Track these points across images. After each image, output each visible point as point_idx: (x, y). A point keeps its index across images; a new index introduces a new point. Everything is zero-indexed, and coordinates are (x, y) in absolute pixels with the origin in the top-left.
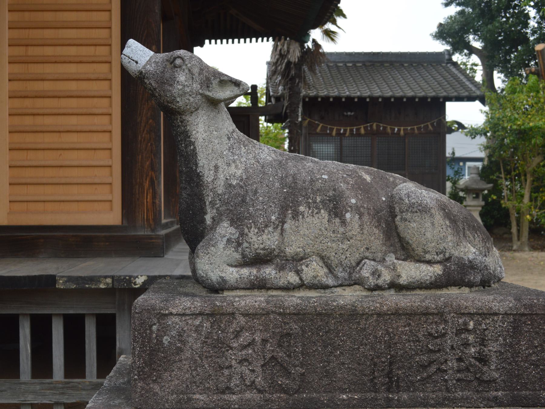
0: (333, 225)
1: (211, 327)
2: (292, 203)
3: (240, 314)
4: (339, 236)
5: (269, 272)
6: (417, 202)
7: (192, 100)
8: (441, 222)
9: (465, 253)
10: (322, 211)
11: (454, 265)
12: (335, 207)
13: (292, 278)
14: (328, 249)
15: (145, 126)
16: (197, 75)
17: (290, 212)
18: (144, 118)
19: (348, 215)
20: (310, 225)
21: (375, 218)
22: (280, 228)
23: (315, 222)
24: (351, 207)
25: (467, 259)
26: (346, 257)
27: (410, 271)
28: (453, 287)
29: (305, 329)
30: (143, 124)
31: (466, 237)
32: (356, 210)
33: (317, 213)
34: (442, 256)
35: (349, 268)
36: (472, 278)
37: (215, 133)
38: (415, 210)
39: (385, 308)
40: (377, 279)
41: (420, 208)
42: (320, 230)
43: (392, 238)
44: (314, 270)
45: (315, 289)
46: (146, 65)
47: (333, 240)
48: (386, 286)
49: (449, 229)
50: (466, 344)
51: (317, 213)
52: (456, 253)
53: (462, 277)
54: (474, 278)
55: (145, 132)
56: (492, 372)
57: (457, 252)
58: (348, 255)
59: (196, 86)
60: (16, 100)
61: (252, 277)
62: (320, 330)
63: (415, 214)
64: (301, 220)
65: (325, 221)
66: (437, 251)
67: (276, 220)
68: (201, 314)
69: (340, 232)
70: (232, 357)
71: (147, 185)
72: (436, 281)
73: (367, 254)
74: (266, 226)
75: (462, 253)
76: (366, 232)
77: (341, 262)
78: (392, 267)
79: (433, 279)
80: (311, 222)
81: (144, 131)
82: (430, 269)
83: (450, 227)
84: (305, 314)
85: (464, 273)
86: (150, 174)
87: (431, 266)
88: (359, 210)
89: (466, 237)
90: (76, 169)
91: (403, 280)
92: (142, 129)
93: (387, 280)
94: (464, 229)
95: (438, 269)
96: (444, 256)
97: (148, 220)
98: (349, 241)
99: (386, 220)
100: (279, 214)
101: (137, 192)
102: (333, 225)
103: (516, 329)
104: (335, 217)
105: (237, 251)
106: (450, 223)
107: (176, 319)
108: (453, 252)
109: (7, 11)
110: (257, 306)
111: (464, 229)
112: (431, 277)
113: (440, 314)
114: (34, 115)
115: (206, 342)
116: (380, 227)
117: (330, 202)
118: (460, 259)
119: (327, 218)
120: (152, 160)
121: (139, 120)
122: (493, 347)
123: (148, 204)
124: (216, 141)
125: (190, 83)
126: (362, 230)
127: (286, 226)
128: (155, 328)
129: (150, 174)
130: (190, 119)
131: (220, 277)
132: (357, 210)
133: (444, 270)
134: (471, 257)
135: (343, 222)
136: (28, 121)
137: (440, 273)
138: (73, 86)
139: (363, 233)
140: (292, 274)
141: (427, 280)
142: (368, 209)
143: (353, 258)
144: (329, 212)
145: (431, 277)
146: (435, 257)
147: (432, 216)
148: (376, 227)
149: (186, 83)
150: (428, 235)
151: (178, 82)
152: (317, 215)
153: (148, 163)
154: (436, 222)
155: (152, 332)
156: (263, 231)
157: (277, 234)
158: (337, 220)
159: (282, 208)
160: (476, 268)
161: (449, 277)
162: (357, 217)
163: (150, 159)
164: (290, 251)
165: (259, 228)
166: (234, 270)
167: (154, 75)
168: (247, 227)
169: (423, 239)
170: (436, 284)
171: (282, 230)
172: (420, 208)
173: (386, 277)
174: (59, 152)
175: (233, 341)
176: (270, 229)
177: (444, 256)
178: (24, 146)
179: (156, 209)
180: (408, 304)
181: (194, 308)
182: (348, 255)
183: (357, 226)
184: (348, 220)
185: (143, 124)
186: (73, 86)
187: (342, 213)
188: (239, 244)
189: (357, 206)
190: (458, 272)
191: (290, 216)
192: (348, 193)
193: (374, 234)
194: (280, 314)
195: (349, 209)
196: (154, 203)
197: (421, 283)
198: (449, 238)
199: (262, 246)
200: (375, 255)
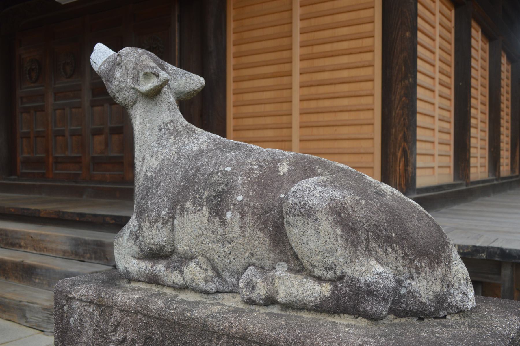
0: (213, 225)
1: (100, 316)
2: (183, 198)
3: (117, 309)
4: (218, 237)
5: (160, 268)
6: (300, 203)
7: (127, 94)
8: (329, 229)
9: (361, 274)
10: (204, 208)
11: (346, 287)
12: (218, 205)
13: (176, 278)
14: (210, 251)
15: (399, 103)
16: (131, 70)
17: (179, 207)
18: (398, 97)
19: (229, 215)
20: (191, 222)
21: (260, 219)
22: (170, 223)
23: (196, 220)
24: (234, 205)
25: (363, 281)
26: (230, 261)
27: (292, 286)
28: (346, 315)
29: (165, 335)
30: (397, 102)
31: (370, 252)
32: (239, 208)
33: (199, 210)
34: (332, 273)
35: (237, 274)
36: (369, 308)
37: (148, 125)
38: (297, 212)
39: (233, 330)
40: (251, 292)
41: (303, 210)
42: (200, 229)
43: (281, 244)
44: (194, 272)
45: (195, 292)
46: (101, 66)
47: (213, 242)
48: (261, 302)
49: (339, 240)
51: (199, 210)
52: (349, 272)
53: (354, 305)
54: (372, 308)
55: (399, 108)
57: (350, 270)
58: (232, 260)
59: (129, 81)
61: (148, 272)
62: (177, 340)
63: (297, 218)
64: (185, 216)
65: (205, 219)
66: (325, 266)
67: (166, 215)
68: (91, 302)
69: (219, 233)
71: (399, 154)
72: (321, 304)
73: (253, 260)
74: (156, 221)
75: (358, 273)
76: (247, 235)
77: (226, 266)
78: (271, 280)
79: (318, 301)
80: (193, 220)
81: (397, 108)
82: (317, 287)
83: (341, 237)
84: (165, 320)
85: (358, 299)
86: (403, 145)
87: (320, 284)
88: (242, 209)
89: (370, 252)
91: (281, 297)
92: (396, 106)
93: (261, 294)
94: (368, 240)
95: (326, 289)
96: (335, 273)
98: (230, 243)
99: (275, 222)
100: (170, 209)
101: (391, 160)
102: (213, 225)
104: (215, 216)
105: (135, 244)
106: (343, 231)
107: (78, 303)
108: (345, 269)
109: (299, 21)
110: (128, 304)
111: (368, 240)
112: (316, 298)
115: (97, 330)
116: (266, 230)
117: (215, 198)
118: (354, 280)
119: (207, 216)
120: (404, 132)
121: (393, 98)
123: (401, 171)
124: (148, 133)
125: (125, 78)
126: (243, 232)
127: (176, 222)
128: (65, 308)
129: (403, 145)
130: (132, 112)
131: (125, 268)
133: (333, 292)
134: (370, 278)
135: (223, 222)
136: (313, 104)
137: (328, 295)
138: (345, 74)
139: (244, 236)
140: (177, 274)
141: (311, 301)
142: (255, 208)
143: (238, 263)
144: (211, 210)
145: (316, 298)
146: (325, 273)
147: (316, 221)
148: (260, 230)
149: (121, 79)
150: (312, 245)
151: (115, 79)
152: (199, 212)
153: (400, 135)
154: (321, 230)
155: (63, 313)
156: (153, 226)
157: (165, 232)
158: (217, 219)
159: (174, 202)
160: (375, 295)
161: (337, 302)
162: (239, 216)
163: (403, 133)
165: (150, 223)
166: (135, 261)
167: (104, 74)
168: (143, 220)
169: (306, 249)
171: (173, 225)
172: (303, 210)
174: (335, 128)
175: (112, 334)
176: (159, 224)
177: (335, 273)
179: (408, 175)
180: (257, 331)
181: (88, 296)
182: (232, 260)
183: (237, 227)
184: (228, 220)
185: (397, 102)
186: (345, 74)
187: (223, 212)
188: (137, 238)
189: (242, 205)
190: (350, 297)
191: (178, 211)
192: (240, 187)
193: (258, 238)
194: (145, 315)
195: (232, 207)
196: (406, 170)
197: (305, 304)
198: (339, 252)
199: (152, 241)
200: (263, 262)
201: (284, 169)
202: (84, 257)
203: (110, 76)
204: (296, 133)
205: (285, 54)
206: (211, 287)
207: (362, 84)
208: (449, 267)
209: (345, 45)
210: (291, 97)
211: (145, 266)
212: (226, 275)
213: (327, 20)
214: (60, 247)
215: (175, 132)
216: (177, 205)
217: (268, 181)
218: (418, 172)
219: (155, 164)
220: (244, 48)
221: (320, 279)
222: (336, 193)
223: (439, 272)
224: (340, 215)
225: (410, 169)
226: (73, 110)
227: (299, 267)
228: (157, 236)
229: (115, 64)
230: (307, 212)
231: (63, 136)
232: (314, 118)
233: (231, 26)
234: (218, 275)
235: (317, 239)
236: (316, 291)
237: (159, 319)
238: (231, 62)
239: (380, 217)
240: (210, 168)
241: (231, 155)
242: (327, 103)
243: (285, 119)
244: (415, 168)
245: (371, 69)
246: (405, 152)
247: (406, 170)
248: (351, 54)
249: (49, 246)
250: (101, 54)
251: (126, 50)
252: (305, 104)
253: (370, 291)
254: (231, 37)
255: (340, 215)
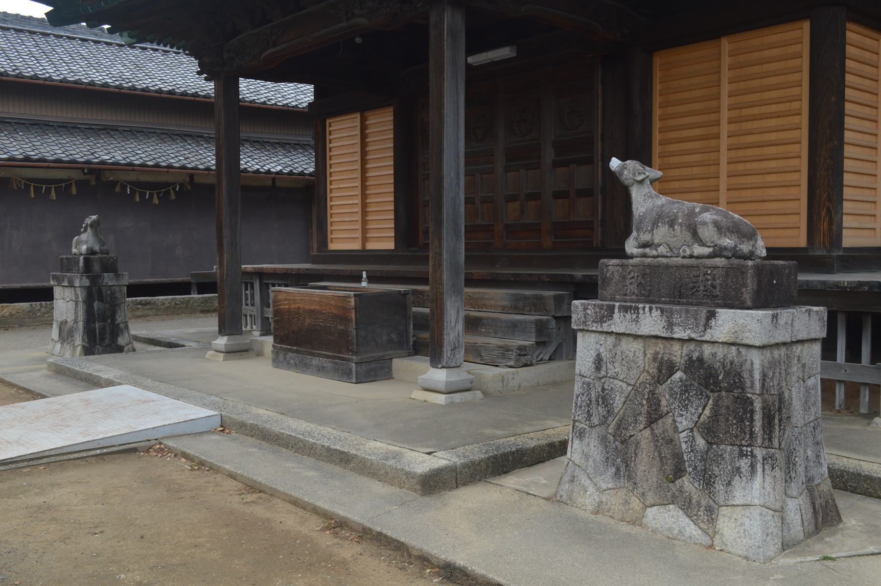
5: (647, 250)
13: (654, 253)
44: (662, 250)
50: (707, 280)
56: (717, 292)
60: (732, 151)
70: (628, 282)
71: (823, 213)
90: (775, 203)
91: (695, 254)
95: (711, 250)
97: (824, 243)
103: (727, 275)
113: (698, 267)
114: (745, 162)
122: (718, 281)
132: (681, 225)
135: (674, 230)
136: (741, 167)
138: (773, 136)
157: (650, 236)
164: (656, 241)
170: (710, 256)
173: (688, 253)
174: (763, 190)
178: (737, 187)
186: (773, 136)
196: (830, 229)
201: (697, 210)
202: (523, 310)
203: (621, 174)
204: (723, 196)
205: (713, 117)
206: (669, 254)
207: (790, 146)
208: (756, 242)
209: (773, 108)
210: (719, 160)
211: (640, 250)
212: (674, 250)
213: (756, 83)
214: (499, 303)
215: (651, 197)
216: (655, 224)
217: (692, 214)
218: (845, 232)
219: (644, 210)
220: (670, 110)
221: (709, 247)
222: (715, 217)
223: (751, 243)
224: (716, 224)
225: (834, 228)
226: (484, 176)
227: (703, 244)
228: (645, 237)
229: (623, 168)
230: (704, 223)
231: (474, 203)
232: (742, 180)
233: (657, 87)
234: (671, 250)
235: (707, 233)
236: (706, 251)
237: (649, 266)
238: (657, 124)
239: (730, 224)
240: (668, 211)
241: (676, 205)
242: (755, 166)
243: (712, 182)
244: (841, 228)
245: (798, 131)
246: (829, 211)
247: (830, 229)
248: (779, 117)
249: (487, 302)
250: (615, 163)
251: (628, 162)
252: (733, 167)
253: (725, 248)
254: (657, 99)
255: (716, 224)
